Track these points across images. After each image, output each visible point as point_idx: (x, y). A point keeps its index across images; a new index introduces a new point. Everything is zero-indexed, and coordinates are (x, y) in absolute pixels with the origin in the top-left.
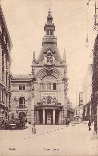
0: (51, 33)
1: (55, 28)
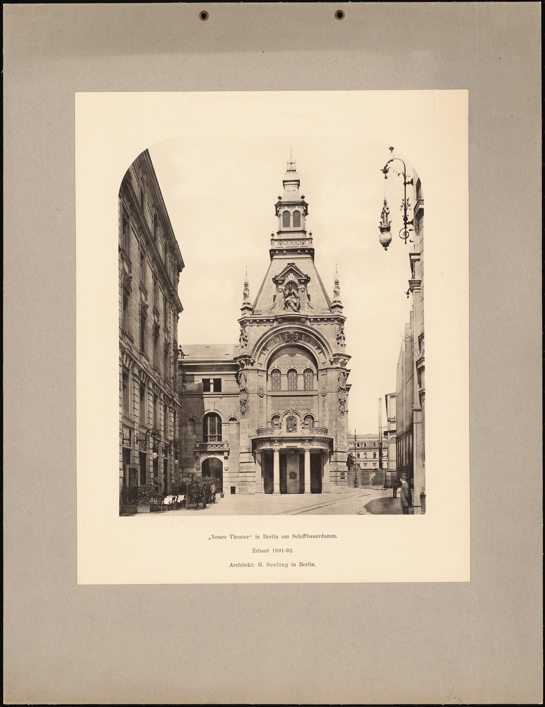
0: (297, 223)
1: (307, 208)
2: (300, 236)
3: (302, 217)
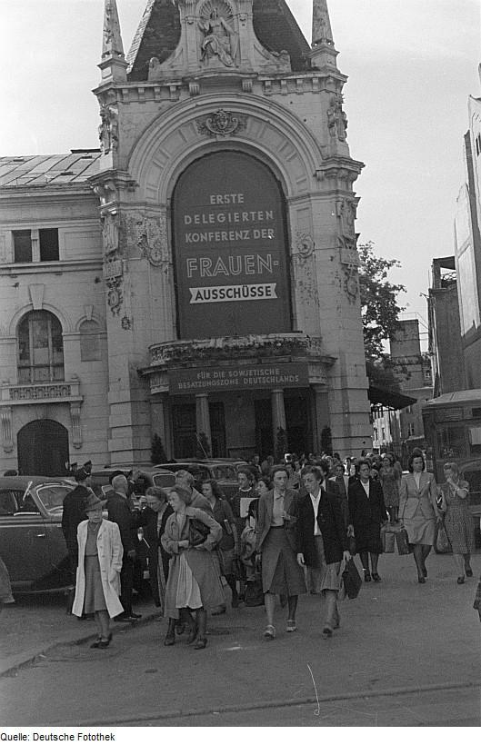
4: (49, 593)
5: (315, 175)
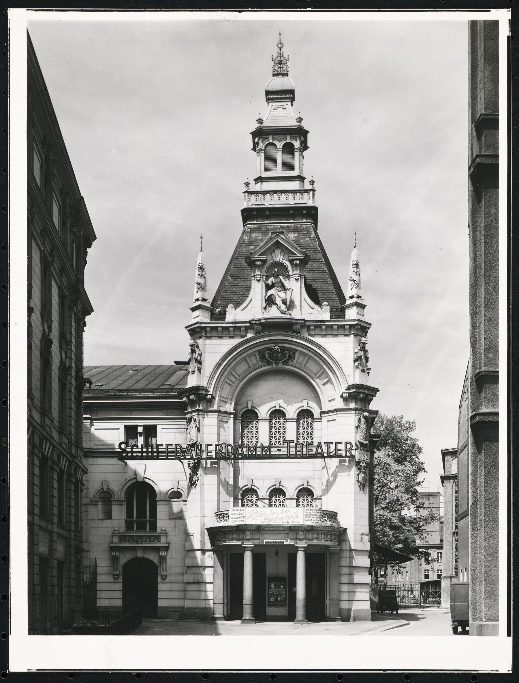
0: (288, 164)
2: (295, 185)
3: (297, 154)
4: (472, 547)
5: (342, 396)
